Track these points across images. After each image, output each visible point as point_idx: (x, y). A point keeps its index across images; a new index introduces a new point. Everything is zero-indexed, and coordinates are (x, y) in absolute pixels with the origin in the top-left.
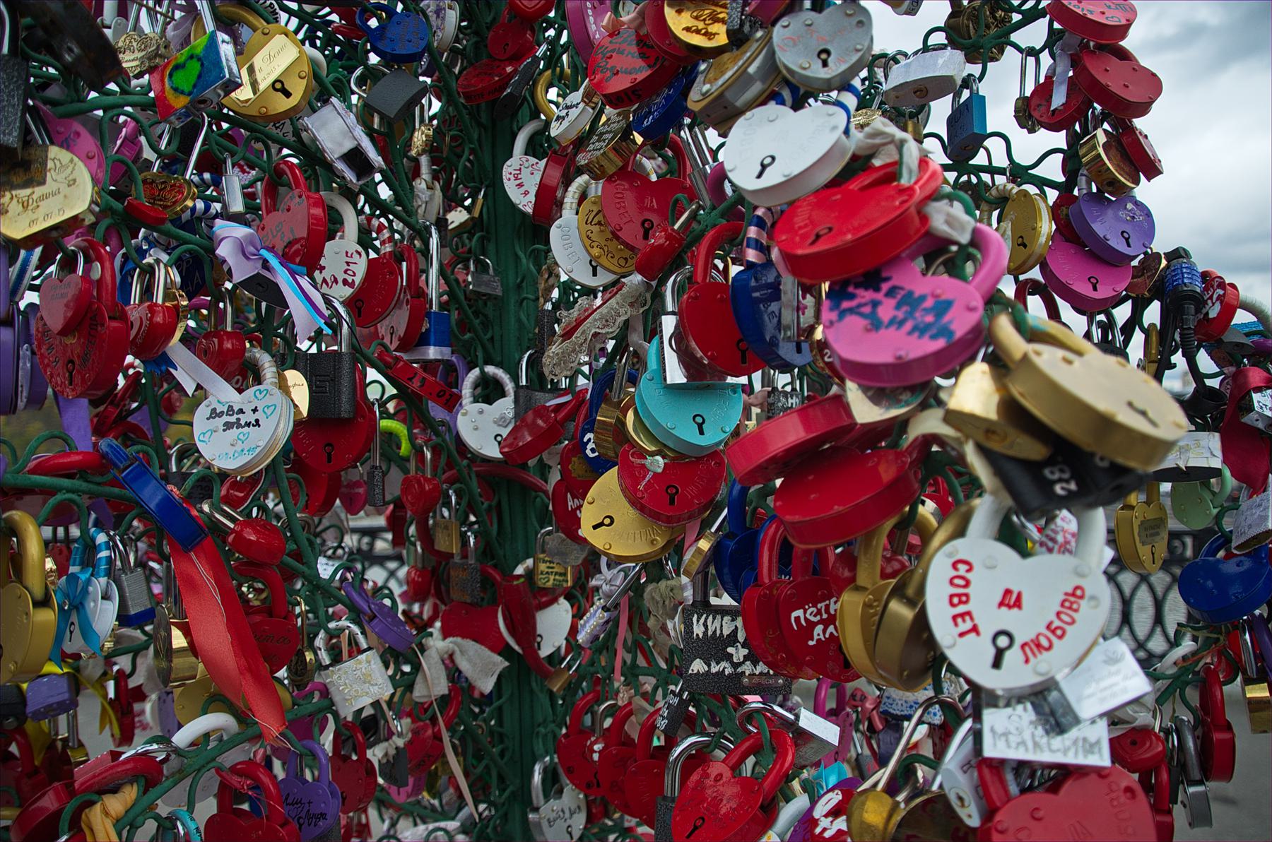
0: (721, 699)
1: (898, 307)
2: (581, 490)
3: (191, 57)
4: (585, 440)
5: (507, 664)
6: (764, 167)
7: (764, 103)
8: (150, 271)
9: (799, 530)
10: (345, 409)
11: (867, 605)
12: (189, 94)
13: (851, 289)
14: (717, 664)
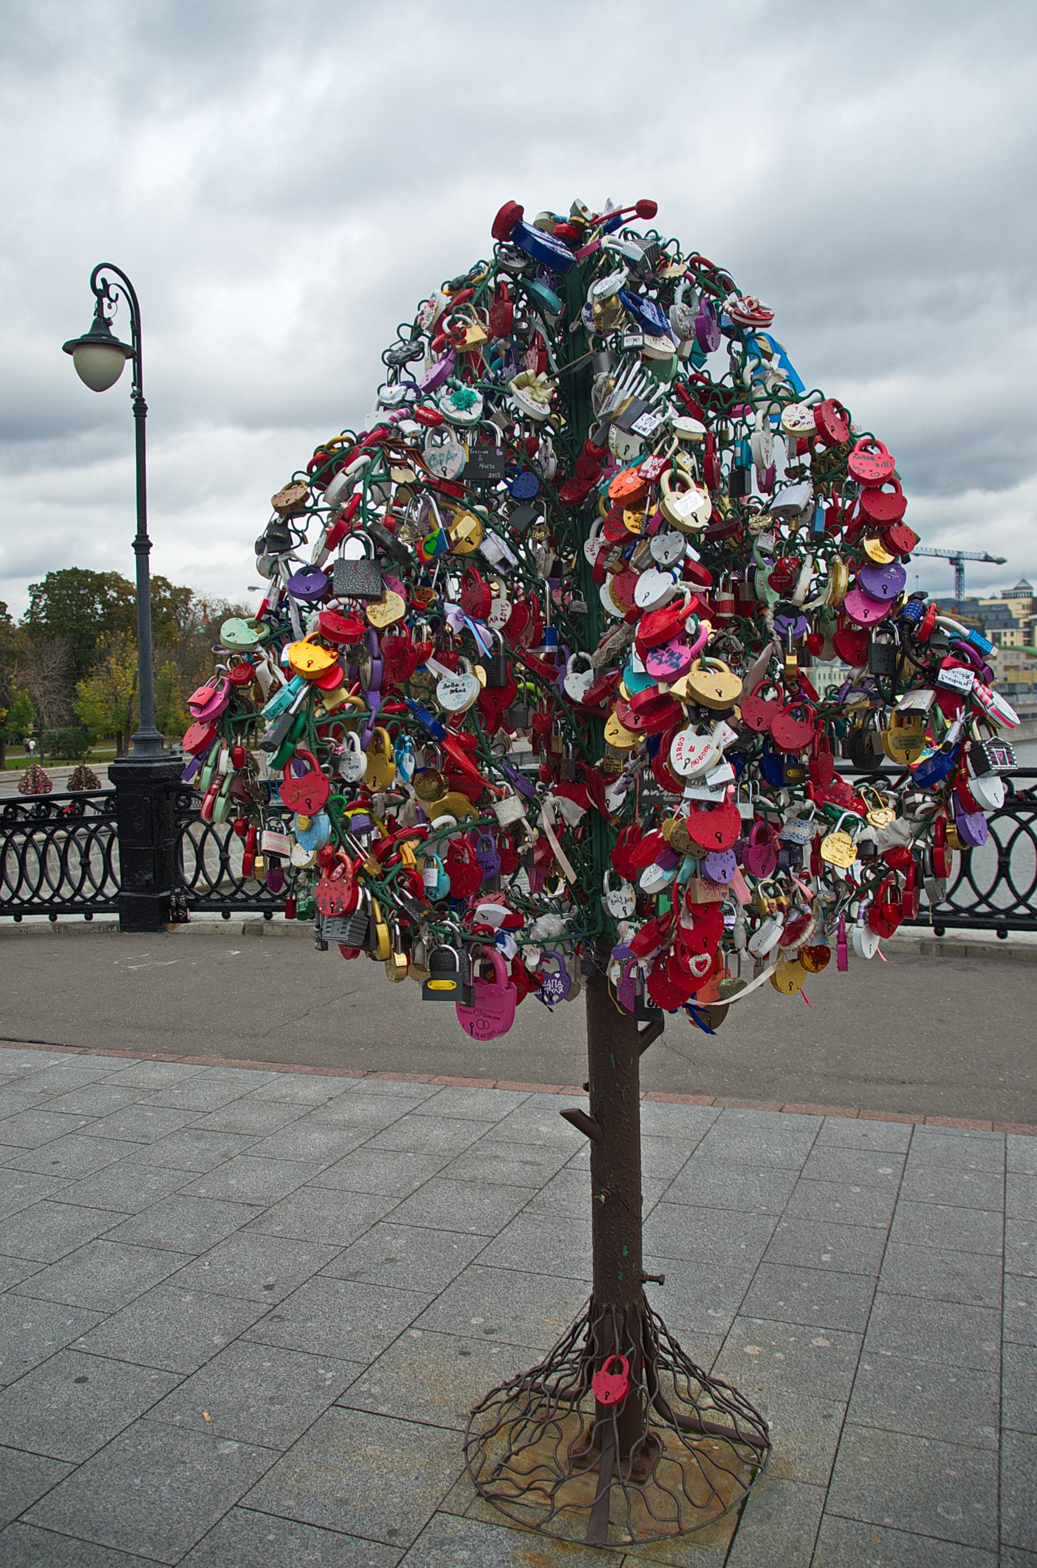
8: (420, 629)
10: (503, 682)
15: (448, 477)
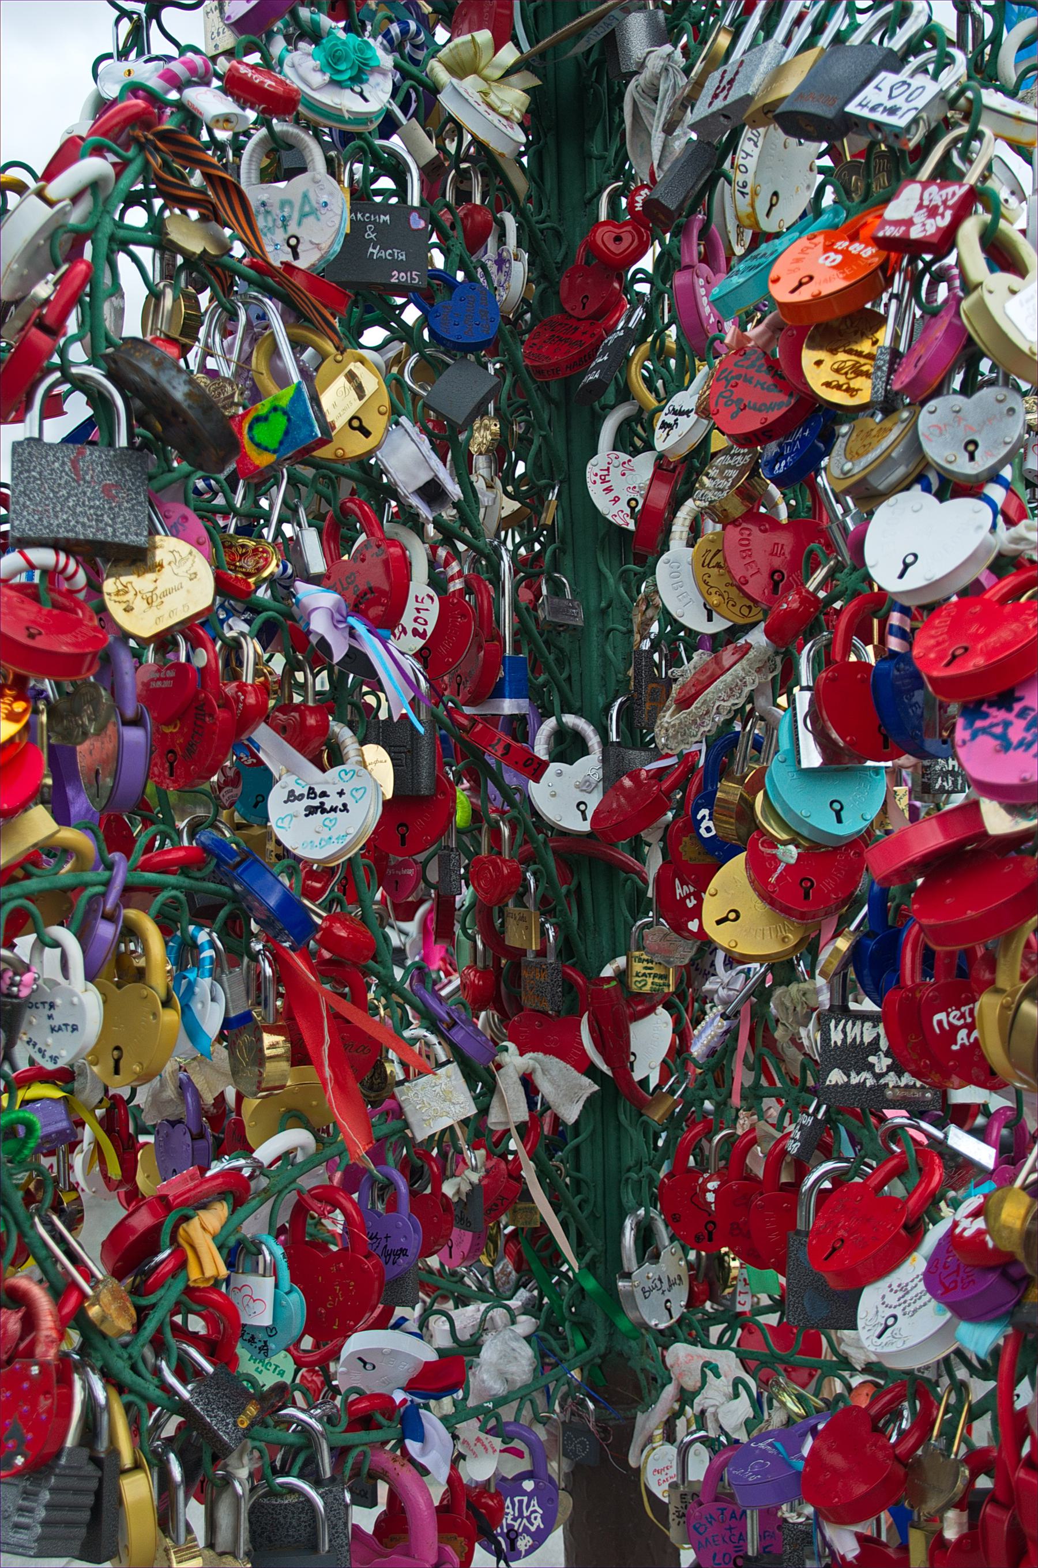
0: (861, 1118)
1: (1028, 729)
2: (702, 879)
3: (275, 409)
4: (699, 817)
5: (596, 1088)
6: (906, 566)
7: (907, 488)
9: (937, 934)
11: (1005, 1007)
12: (275, 452)
13: (984, 708)
14: (858, 1074)
15: (302, 264)
